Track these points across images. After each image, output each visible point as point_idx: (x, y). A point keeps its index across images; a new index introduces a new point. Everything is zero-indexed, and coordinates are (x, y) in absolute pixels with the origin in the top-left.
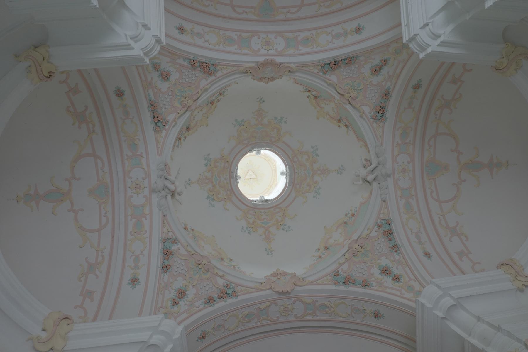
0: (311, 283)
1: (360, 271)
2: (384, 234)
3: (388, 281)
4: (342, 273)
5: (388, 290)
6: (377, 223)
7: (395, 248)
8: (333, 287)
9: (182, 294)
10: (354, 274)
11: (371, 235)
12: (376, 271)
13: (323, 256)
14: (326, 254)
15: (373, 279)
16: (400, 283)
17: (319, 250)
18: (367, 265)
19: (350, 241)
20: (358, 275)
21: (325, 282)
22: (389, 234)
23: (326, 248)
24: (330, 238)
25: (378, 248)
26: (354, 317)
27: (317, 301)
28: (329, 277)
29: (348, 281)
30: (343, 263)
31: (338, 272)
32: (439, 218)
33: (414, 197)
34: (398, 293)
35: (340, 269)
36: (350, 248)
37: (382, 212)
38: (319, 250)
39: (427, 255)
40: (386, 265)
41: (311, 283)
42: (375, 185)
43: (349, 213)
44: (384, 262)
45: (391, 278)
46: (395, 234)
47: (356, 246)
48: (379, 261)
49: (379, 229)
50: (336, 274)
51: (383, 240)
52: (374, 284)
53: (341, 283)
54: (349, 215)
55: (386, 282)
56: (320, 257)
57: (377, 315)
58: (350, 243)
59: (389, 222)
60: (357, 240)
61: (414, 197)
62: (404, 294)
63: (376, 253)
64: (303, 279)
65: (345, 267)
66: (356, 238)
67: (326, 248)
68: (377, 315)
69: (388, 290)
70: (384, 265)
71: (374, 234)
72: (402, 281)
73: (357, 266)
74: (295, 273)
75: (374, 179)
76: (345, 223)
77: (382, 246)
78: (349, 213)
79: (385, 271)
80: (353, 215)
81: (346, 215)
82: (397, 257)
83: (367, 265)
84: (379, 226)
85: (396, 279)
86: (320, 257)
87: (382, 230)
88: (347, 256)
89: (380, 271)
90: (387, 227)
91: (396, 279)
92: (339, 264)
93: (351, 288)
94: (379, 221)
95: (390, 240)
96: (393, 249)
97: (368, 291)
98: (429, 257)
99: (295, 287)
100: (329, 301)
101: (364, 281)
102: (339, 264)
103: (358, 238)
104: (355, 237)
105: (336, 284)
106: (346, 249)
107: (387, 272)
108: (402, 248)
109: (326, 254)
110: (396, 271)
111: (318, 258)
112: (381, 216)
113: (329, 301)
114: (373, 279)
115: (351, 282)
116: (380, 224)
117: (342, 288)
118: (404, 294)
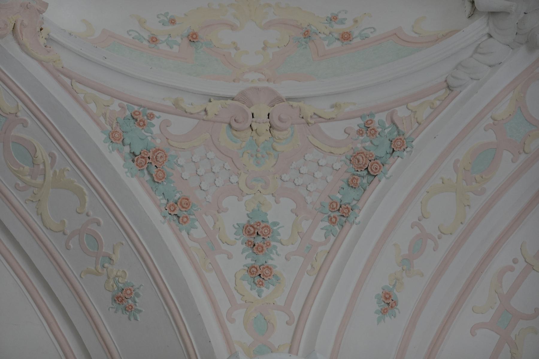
0: (58, 73)
1: (201, 171)
2: (354, 158)
3: (236, 259)
4: (156, 130)
5: (211, 278)
6: (372, 115)
7: (340, 213)
8: (98, 137)
9: (256, 235)
10: (181, 161)
11: (323, 126)
12: (236, 212)
13: (163, 47)
14: (176, 48)
15: (209, 220)
16: (254, 293)
17: (173, 21)
18: (234, 179)
19: (265, 84)
20: (185, 175)
21: (92, 107)
22: (366, 169)
23: (193, 38)
24: (233, 27)
25: (304, 170)
26: (68, 248)
27: (24, 124)
28: (115, 106)
29: (149, 162)
30: (186, 114)
31: (151, 117)
32: (515, 261)
33: (523, 157)
34: (224, 306)
35: (164, 116)
36: (243, 98)
37: (411, 105)
38: (173, 21)
39: (388, 303)
40: (275, 224)
41: (58, 73)
42: (479, 26)
43: (342, 22)
44: (280, 213)
45: (249, 262)
46: (379, 185)
47: (261, 110)
48: (270, 199)
49: (360, 133)
50: (140, 118)
51: (337, 166)
52: (198, 233)
53: (127, 149)
54: (338, 28)
55: (230, 257)
56: (154, 40)
57: (123, 299)
58: (257, 89)
59: (398, 145)
60: (280, 100)
61: (523, 157)
62: (232, 321)
63: (286, 177)
64: (49, 39)
65: (180, 126)
66: (284, 93)
67: (193, 38)
68: (123, 299)
69: (211, 278)
70: (271, 219)
71: (335, 131)
72: (265, 292)
73: (211, 155)
74: (46, 5)
75: (493, 14)
76: (307, 34)
77: (318, 175)
78: (342, 22)
79: (256, 235)
80: (346, 37)
81: (334, 18)
82: (318, 235)
83: (234, 179)
84: (367, 129)
85: (259, 275)
86: (154, 40)
87: (361, 143)
88: (214, 107)
89: (244, 220)
90: (381, 152)
91: (259, 275)
92: (176, 103)
93: (136, 185)
94: (381, 117)
95: (352, 184)
96: (332, 209)
97: (166, 230)
98: (384, 312)
99: (10, 37)
100: (52, 156)
101: (185, 203)
102: (176, 103)
103: (288, 99)
104: (285, 89)
105: (115, 138)
106: (233, 90)
107: (259, 241)
108: (354, 227)
109: (176, 48)
110: (277, 260)
111: (146, 36)
112: (401, 112)
113: (52, 156)
114: (209, 220)
115: (154, 170)
116: (376, 125)
117: (117, 160)
118: (232, 321)
